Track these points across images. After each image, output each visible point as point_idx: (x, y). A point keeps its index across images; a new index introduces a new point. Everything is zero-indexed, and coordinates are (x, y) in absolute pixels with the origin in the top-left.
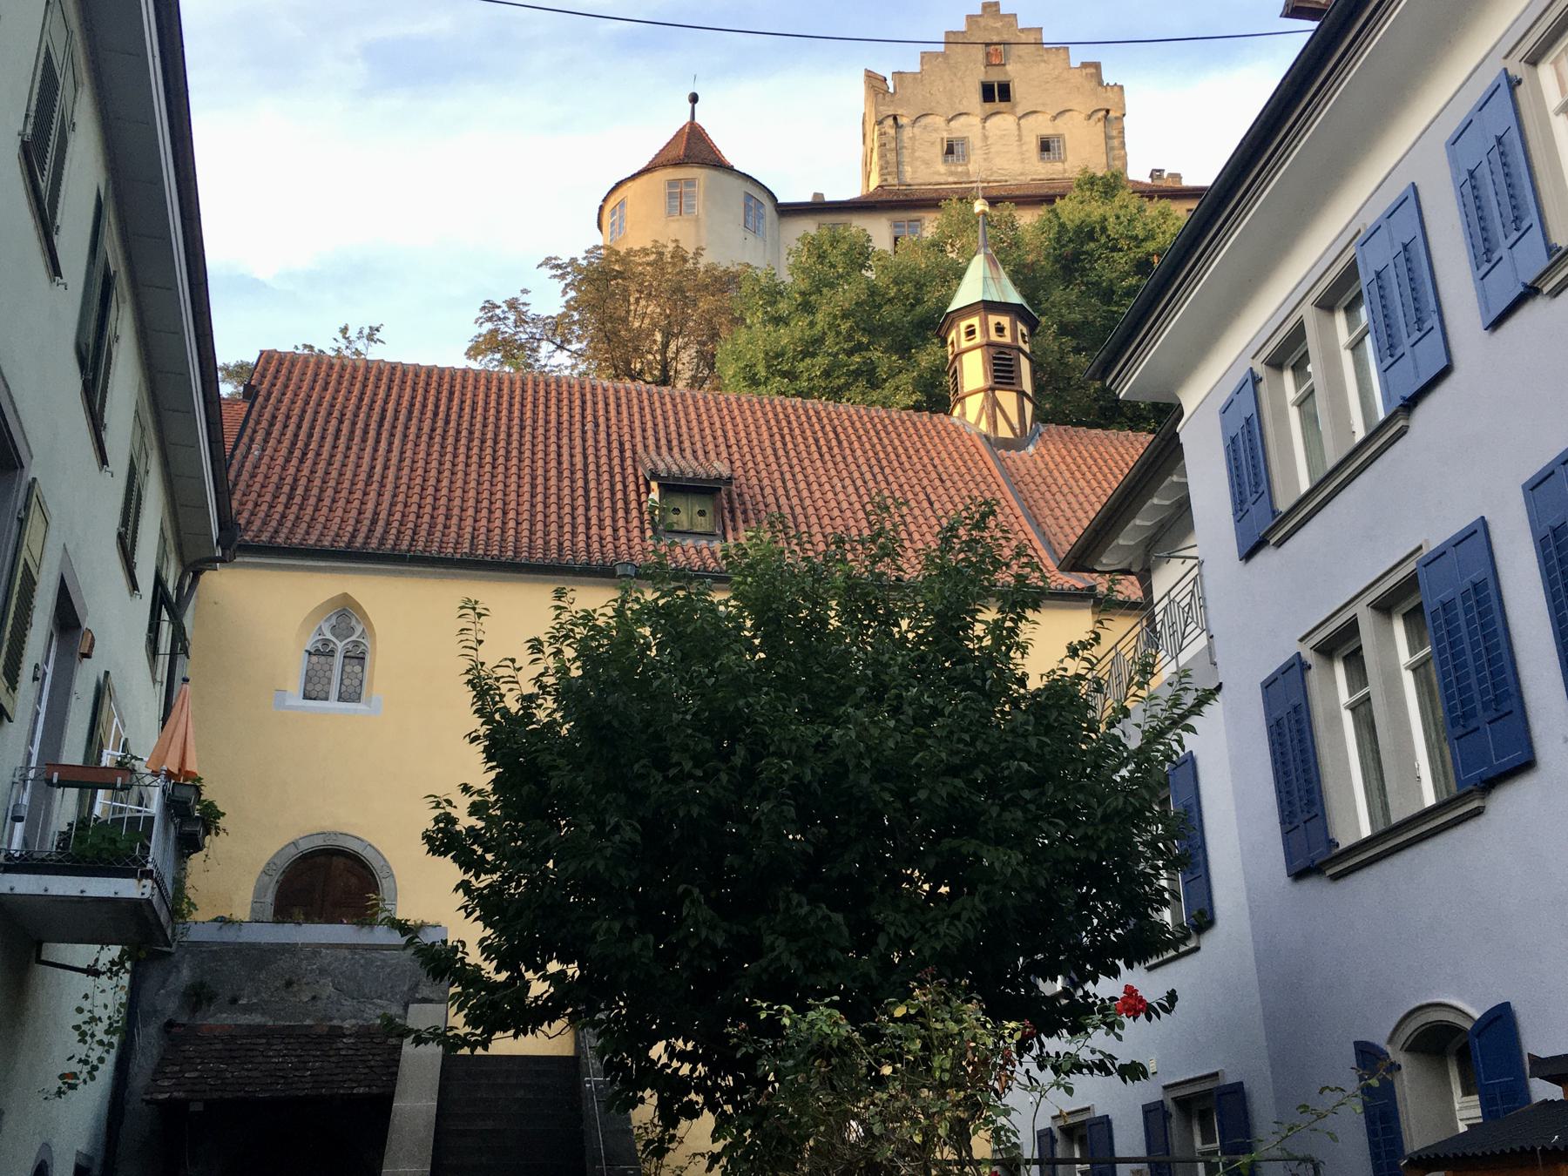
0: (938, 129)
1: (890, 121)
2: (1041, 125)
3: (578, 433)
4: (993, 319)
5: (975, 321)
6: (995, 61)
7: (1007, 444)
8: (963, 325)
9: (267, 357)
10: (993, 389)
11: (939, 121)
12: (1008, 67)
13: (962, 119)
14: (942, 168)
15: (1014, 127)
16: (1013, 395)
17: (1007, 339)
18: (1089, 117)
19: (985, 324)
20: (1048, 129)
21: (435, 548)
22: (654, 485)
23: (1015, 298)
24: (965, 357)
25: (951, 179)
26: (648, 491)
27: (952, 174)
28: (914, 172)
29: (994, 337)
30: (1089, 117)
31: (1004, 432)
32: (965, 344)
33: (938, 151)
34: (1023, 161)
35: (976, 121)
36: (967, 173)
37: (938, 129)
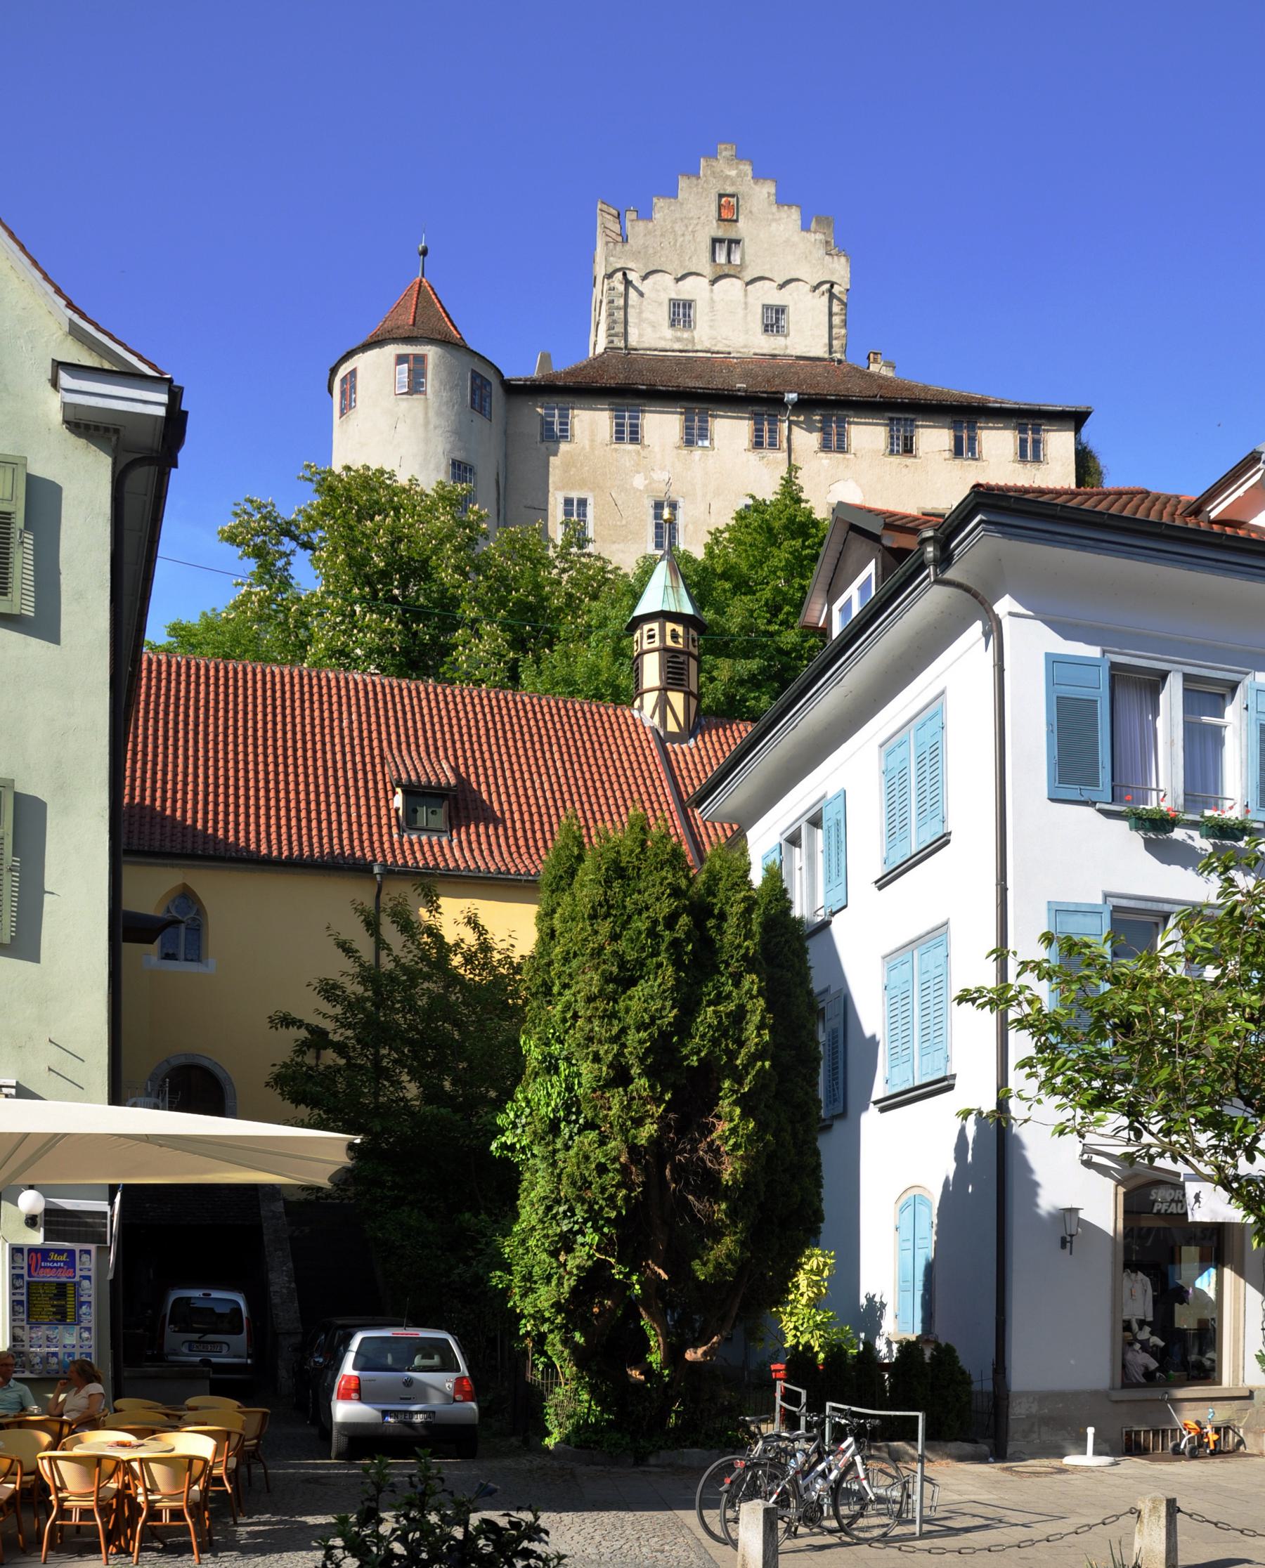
0: (661, 290)
1: (619, 275)
2: (767, 294)
3: (336, 731)
4: (670, 626)
5: (655, 626)
6: (725, 215)
7: (673, 737)
8: (646, 627)
9: (1036, 1185)
10: (666, 690)
11: (668, 280)
12: (740, 224)
13: (691, 279)
14: (668, 333)
15: (742, 293)
16: (681, 695)
17: (680, 645)
18: (815, 288)
19: (662, 630)
20: (776, 298)
21: (189, 845)
22: (398, 790)
23: (688, 609)
24: (646, 657)
25: (677, 346)
26: (394, 793)
27: (678, 340)
28: (641, 335)
29: (670, 643)
30: (815, 288)
31: (672, 727)
32: (646, 646)
33: (663, 314)
34: (747, 332)
35: (704, 282)
36: (693, 341)
37: (661, 290)
